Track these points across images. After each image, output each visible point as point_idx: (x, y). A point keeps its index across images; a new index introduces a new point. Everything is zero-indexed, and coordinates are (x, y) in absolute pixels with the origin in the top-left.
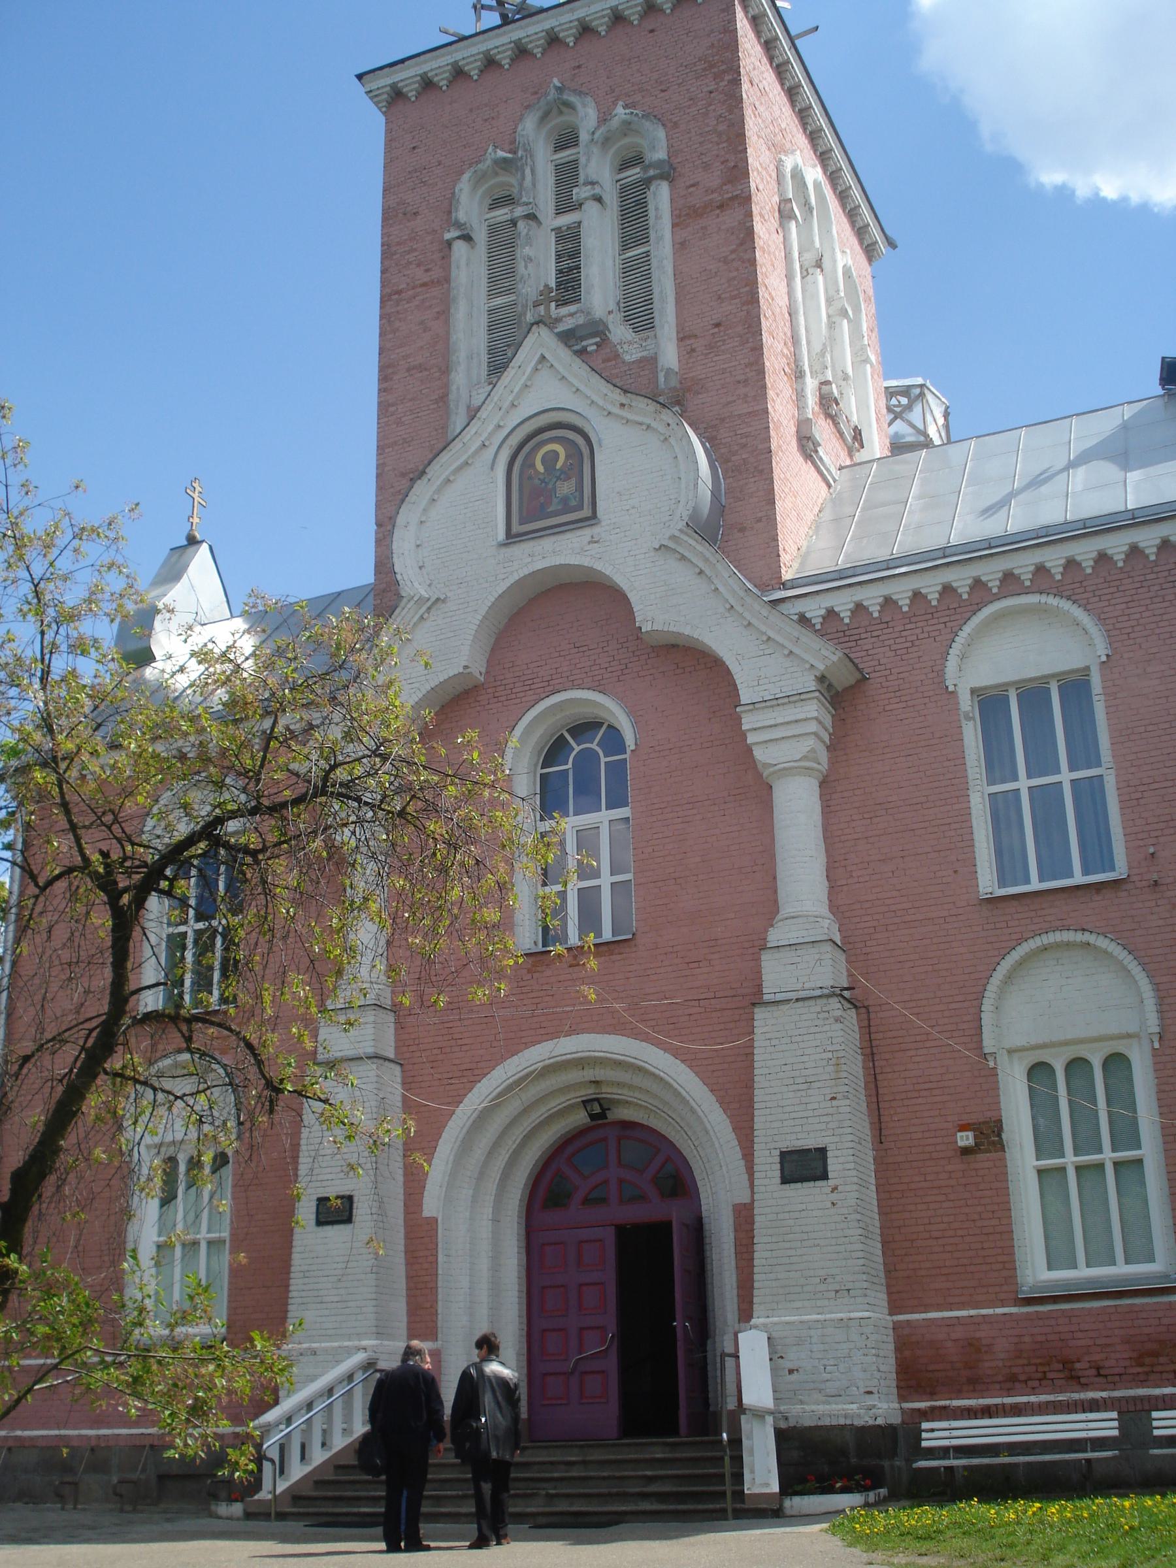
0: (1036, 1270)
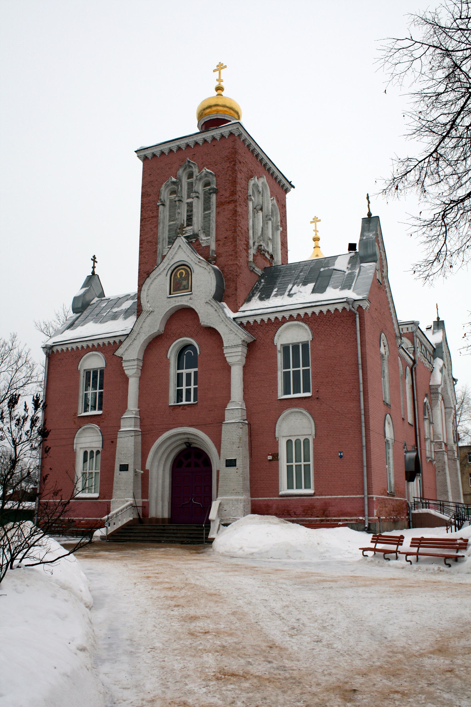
0: (284, 490)
